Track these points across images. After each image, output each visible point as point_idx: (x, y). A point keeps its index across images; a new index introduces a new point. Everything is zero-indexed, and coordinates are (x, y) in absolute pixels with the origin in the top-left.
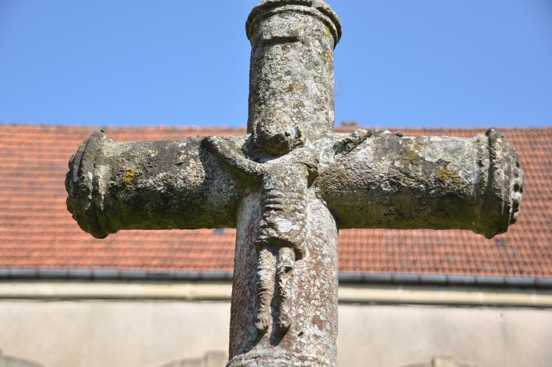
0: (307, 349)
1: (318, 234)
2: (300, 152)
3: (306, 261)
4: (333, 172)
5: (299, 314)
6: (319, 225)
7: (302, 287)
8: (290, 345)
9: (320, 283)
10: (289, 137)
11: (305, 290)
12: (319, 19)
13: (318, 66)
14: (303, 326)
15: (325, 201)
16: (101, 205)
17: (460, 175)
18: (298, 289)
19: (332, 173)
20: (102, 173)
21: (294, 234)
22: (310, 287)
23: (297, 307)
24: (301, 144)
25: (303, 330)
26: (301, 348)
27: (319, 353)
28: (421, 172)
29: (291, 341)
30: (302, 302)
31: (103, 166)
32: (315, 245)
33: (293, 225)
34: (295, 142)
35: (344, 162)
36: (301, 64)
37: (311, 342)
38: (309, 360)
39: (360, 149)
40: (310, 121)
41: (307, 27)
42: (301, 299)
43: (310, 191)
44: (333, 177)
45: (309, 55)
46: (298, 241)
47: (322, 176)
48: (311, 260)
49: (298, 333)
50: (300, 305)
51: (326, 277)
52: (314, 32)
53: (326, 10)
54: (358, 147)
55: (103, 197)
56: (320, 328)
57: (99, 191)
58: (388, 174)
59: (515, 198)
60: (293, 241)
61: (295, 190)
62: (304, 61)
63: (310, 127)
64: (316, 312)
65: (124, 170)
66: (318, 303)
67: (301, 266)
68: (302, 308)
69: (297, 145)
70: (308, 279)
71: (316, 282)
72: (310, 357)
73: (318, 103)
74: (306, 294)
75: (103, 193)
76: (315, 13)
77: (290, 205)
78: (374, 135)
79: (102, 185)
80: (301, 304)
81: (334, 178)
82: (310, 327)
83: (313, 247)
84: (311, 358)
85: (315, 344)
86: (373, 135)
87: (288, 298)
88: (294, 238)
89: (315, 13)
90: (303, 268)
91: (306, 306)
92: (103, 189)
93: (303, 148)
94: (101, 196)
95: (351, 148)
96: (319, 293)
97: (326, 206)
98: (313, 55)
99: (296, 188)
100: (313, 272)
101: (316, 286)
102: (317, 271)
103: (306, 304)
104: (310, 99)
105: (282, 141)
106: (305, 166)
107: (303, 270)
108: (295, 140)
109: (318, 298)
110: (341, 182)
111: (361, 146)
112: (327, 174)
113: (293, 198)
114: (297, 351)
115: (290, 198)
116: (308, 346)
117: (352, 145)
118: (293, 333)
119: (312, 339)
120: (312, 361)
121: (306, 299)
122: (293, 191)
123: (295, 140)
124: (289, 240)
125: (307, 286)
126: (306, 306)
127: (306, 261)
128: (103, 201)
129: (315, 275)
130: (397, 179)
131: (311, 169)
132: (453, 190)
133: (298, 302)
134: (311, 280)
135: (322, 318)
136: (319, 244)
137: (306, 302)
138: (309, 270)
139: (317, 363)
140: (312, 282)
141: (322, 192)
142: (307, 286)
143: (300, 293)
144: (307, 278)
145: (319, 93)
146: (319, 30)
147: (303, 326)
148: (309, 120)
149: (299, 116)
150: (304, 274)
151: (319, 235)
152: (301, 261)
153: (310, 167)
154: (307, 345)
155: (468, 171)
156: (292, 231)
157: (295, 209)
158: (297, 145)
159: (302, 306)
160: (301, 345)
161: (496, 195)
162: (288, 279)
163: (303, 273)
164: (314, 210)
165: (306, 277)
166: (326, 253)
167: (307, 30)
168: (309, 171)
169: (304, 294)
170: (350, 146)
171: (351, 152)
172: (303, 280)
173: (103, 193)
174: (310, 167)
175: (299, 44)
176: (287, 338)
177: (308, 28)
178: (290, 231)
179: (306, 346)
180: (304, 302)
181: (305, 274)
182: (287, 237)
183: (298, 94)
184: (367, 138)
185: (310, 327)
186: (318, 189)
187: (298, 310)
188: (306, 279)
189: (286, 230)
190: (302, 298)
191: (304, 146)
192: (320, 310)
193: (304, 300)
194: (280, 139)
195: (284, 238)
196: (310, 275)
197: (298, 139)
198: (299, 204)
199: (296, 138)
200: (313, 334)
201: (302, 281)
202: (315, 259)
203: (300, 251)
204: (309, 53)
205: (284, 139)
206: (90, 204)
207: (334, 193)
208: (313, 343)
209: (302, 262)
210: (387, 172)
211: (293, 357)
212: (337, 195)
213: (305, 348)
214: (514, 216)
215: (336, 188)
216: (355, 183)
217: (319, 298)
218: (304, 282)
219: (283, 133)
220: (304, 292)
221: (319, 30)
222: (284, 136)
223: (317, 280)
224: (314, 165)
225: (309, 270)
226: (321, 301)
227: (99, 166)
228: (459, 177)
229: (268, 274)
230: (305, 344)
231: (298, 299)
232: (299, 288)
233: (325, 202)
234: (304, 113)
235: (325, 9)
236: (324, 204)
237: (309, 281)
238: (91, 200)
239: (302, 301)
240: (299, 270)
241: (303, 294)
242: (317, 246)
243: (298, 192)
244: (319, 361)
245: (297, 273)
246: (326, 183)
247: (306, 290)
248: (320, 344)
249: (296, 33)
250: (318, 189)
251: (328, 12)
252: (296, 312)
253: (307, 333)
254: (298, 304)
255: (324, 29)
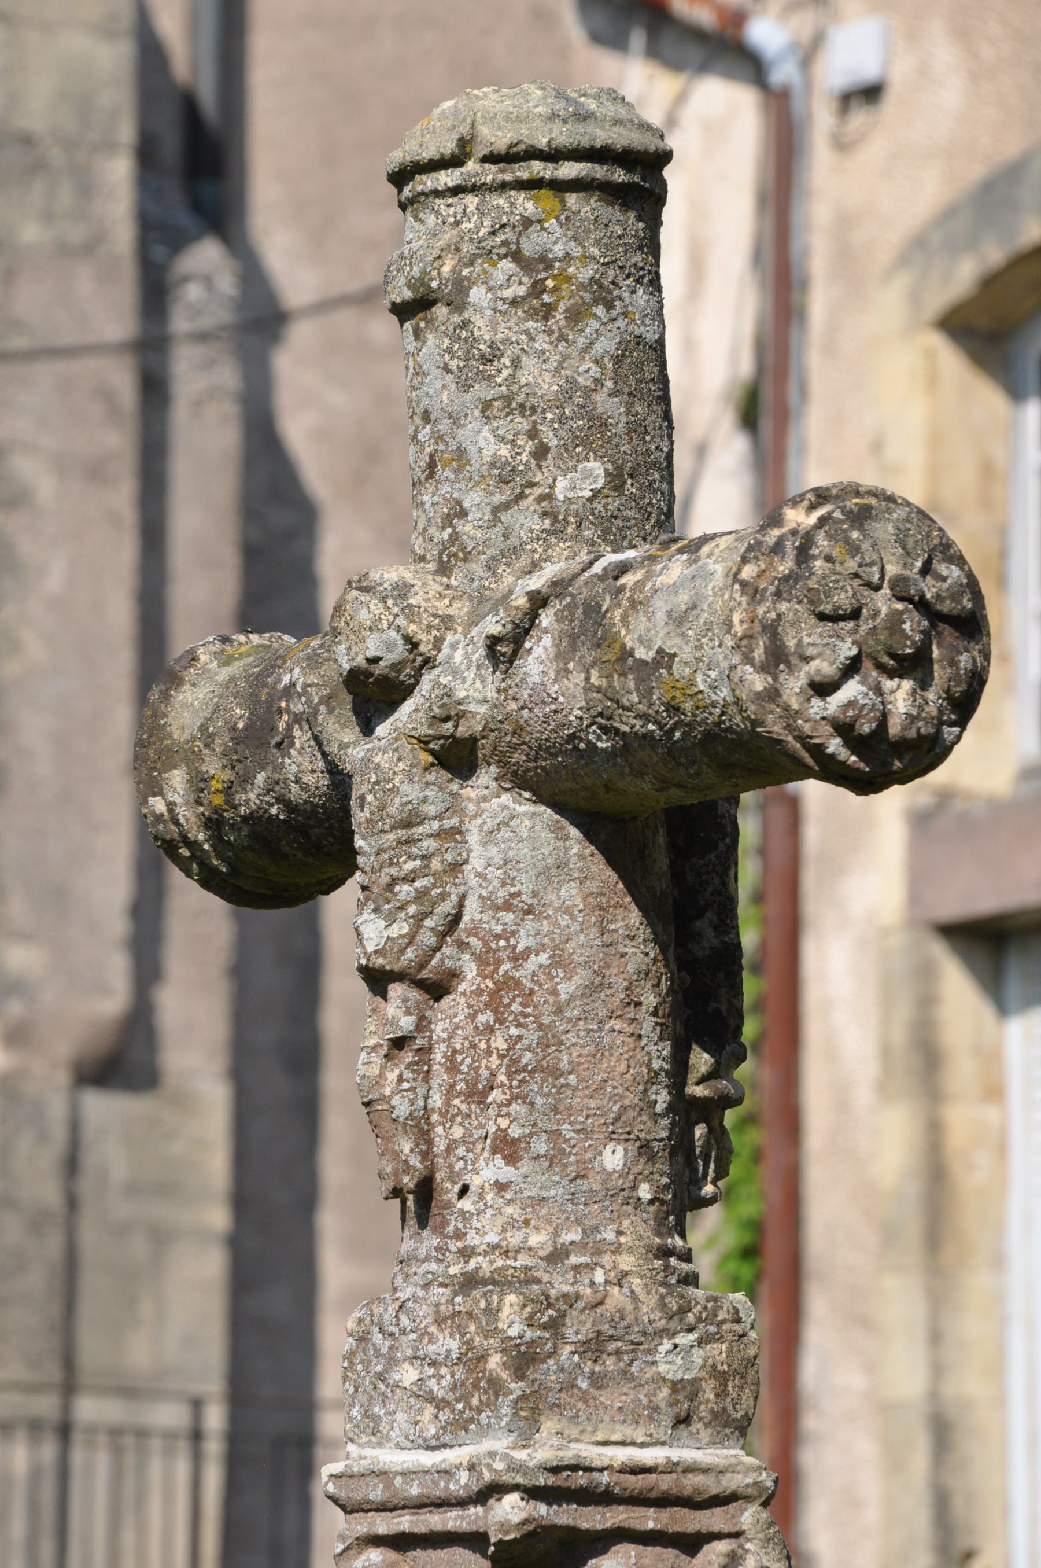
0: (479, 1225)
1: (500, 901)
2: (432, 684)
3: (464, 994)
4: (501, 722)
5: (454, 1140)
6: (505, 872)
7: (455, 1067)
8: (445, 1223)
9: (506, 1040)
10: (381, 663)
11: (463, 1073)
12: (496, 190)
13: (495, 363)
14: (465, 1168)
15: (525, 790)
16: (215, 862)
17: (702, 688)
18: (445, 1077)
19: (499, 726)
20: (179, 790)
21: (396, 950)
22: (477, 1061)
23: (448, 1126)
24: (428, 662)
25: (467, 1178)
26: (465, 1227)
27: (511, 1224)
28: (635, 694)
29: (445, 1212)
30: (459, 1109)
31: (176, 772)
32: (492, 935)
33: (390, 925)
34: (414, 661)
35: (510, 692)
36: (449, 378)
37: (485, 1204)
38: (480, 1254)
39: (531, 649)
40: (484, 553)
41: (462, 238)
42: (456, 1102)
43: (479, 781)
44: (506, 734)
45: (466, 339)
46: (411, 961)
47: (483, 738)
48: (479, 985)
49: (457, 1188)
50: (454, 1116)
51: (526, 1016)
52: (483, 244)
53: (508, 153)
54: (527, 645)
55: (206, 847)
56: (512, 1159)
57: (189, 835)
58: (588, 710)
59: (829, 712)
60: (396, 967)
61: (387, 827)
62: (454, 364)
63: (482, 574)
64: (500, 1119)
65: (206, 776)
66: (504, 1096)
67: (451, 1012)
68: (460, 1124)
69: (422, 667)
70: (470, 1043)
71: (495, 1041)
72: (482, 1244)
73: (507, 483)
74: (467, 1082)
75: (201, 836)
76: (476, 182)
77: (380, 870)
78: (556, 597)
79: (187, 820)
80: (457, 1115)
81: (508, 738)
82: (487, 1165)
83: (486, 944)
84: (484, 1247)
85: (496, 1206)
86: (552, 598)
87: (401, 1119)
88: (398, 959)
89: (476, 182)
90: (456, 1016)
91: (469, 1116)
92: (195, 828)
93: (437, 671)
94: (200, 846)
95: (510, 652)
96: (503, 1070)
97: (534, 802)
98: (476, 333)
99: (388, 821)
100: (486, 1017)
101: (495, 1051)
102: (495, 1011)
103: (470, 1110)
104: (477, 483)
105: (371, 680)
106: (415, 741)
107: (456, 1020)
108: (411, 656)
109: (502, 1082)
110: (524, 743)
111: (532, 636)
112: (492, 731)
113: (385, 851)
114: (459, 1235)
115: (378, 854)
116: (481, 1218)
117: (507, 646)
118: (448, 1191)
119: (489, 1197)
120: (486, 1253)
121: (468, 1097)
122: (383, 831)
123: (411, 656)
124: (388, 968)
125: (469, 1060)
126: (469, 1116)
127: (464, 994)
128: (213, 854)
129: (492, 1023)
130: (610, 718)
131: (431, 746)
132: (707, 724)
133: (448, 1112)
134: (480, 1040)
135: (515, 1132)
136: (504, 930)
137: (468, 1103)
138: (472, 1017)
139: (500, 1254)
140: (483, 1045)
141: (506, 775)
142: (469, 1060)
143: (452, 1086)
144: (466, 1038)
145: (505, 451)
146: (503, 226)
147: (465, 1168)
148: (479, 554)
149: (454, 550)
150: (460, 1032)
151: (506, 902)
152: (452, 997)
153: (427, 743)
154: (478, 1215)
155: (710, 673)
156: (390, 943)
157: (393, 880)
158: (422, 667)
159: (459, 1119)
160: (464, 1219)
161: (760, 733)
162: (403, 1067)
163: (457, 1028)
164: (492, 832)
165: (464, 1039)
166: (530, 944)
167: (465, 247)
168: (432, 752)
169: (461, 1086)
170: (504, 650)
171: (517, 662)
172: (458, 1047)
173: (201, 836)
174: (427, 743)
175: (440, 311)
176: (436, 1206)
177: (466, 238)
178: (386, 943)
179: (475, 1217)
180: (464, 1107)
181: (463, 1029)
182: (381, 961)
183: (447, 479)
184: (540, 611)
185: (487, 1165)
186: (493, 769)
187: (451, 1131)
188: (467, 1044)
189: (375, 943)
190: (457, 1097)
191: (437, 663)
192: (508, 1114)
193: (462, 1102)
194: (362, 677)
195: (377, 966)
196: (476, 1028)
197: (415, 651)
198: (401, 860)
199: (411, 651)
200: (492, 1182)
201: (455, 1052)
202: (492, 977)
203: (429, 982)
204: (464, 334)
205: (372, 675)
206: (195, 865)
207: (528, 770)
208: (492, 1206)
209: (454, 1000)
210: (583, 704)
211: (447, 1254)
212: (537, 774)
213: (475, 1222)
214: (891, 736)
215: (524, 758)
216: (546, 740)
217: (507, 1082)
218: (461, 1053)
219: (360, 661)
220: (461, 1080)
221: (503, 226)
222: (366, 669)
223: (498, 1033)
224: (429, 736)
225: (472, 1017)
226: (511, 1087)
227: (167, 775)
228: (701, 692)
229: (372, 1060)
230: (473, 1214)
231: (447, 1103)
232: (449, 1073)
233: (527, 795)
234: (465, 537)
235: (503, 152)
236: (528, 800)
237: (474, 1046)
238: (189, 858)
239: (459, 1105)
240: (447, 1026)
241: (458, 1088)
242: (498, 937)
243: (396, 828)
244: (505, 1249)
245: (441, 1034)
246: (501, 752)
247: (466, 1073)
248: (509, 1202)
249: (423, 284)
250: (493, 769)
251: (518, 153)
252: (446, 1138)
253: (476, 1182)
254: (449, 1115)
255: (526, 204)
